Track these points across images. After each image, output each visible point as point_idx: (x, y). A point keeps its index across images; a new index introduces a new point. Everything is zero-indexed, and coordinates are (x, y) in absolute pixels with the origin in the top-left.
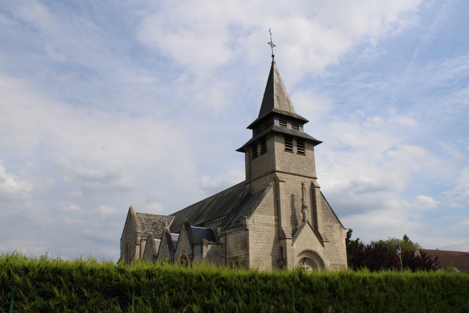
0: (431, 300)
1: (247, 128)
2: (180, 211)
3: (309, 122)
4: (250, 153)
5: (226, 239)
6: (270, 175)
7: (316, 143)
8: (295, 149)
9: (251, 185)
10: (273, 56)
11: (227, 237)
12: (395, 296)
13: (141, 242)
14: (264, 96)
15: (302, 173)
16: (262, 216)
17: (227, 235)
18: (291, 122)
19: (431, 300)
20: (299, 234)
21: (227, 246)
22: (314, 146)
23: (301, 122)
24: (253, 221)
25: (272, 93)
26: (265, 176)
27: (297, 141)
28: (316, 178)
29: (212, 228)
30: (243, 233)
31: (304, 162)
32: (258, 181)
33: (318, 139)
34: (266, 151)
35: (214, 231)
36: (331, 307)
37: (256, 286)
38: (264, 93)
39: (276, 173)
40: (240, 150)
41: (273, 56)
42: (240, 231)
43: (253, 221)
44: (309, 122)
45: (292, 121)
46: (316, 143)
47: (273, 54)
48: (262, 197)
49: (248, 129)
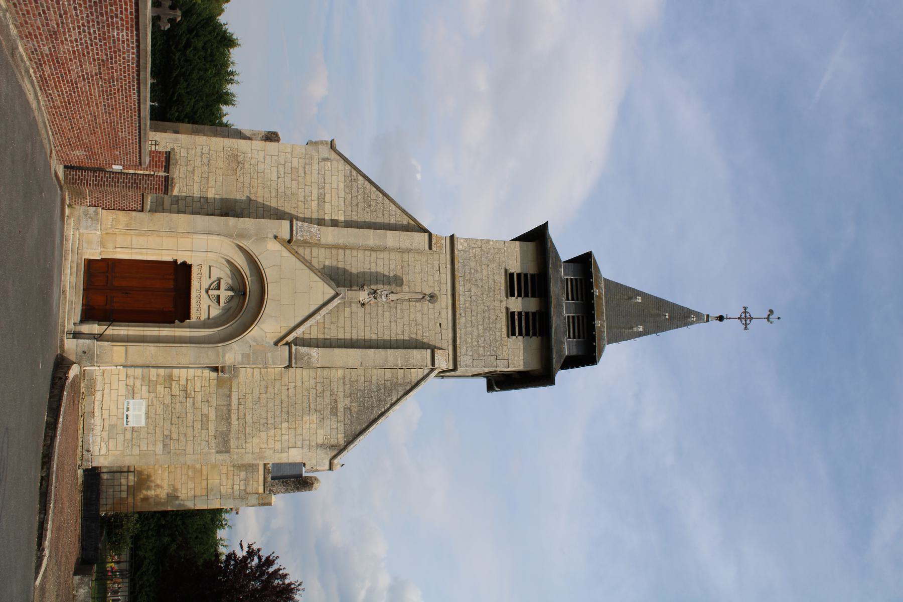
10: (721, 318)
15: (463, 320)
16: (342, 185)
24: (327, 159)
41: (721, 318)
43: (327, 159)
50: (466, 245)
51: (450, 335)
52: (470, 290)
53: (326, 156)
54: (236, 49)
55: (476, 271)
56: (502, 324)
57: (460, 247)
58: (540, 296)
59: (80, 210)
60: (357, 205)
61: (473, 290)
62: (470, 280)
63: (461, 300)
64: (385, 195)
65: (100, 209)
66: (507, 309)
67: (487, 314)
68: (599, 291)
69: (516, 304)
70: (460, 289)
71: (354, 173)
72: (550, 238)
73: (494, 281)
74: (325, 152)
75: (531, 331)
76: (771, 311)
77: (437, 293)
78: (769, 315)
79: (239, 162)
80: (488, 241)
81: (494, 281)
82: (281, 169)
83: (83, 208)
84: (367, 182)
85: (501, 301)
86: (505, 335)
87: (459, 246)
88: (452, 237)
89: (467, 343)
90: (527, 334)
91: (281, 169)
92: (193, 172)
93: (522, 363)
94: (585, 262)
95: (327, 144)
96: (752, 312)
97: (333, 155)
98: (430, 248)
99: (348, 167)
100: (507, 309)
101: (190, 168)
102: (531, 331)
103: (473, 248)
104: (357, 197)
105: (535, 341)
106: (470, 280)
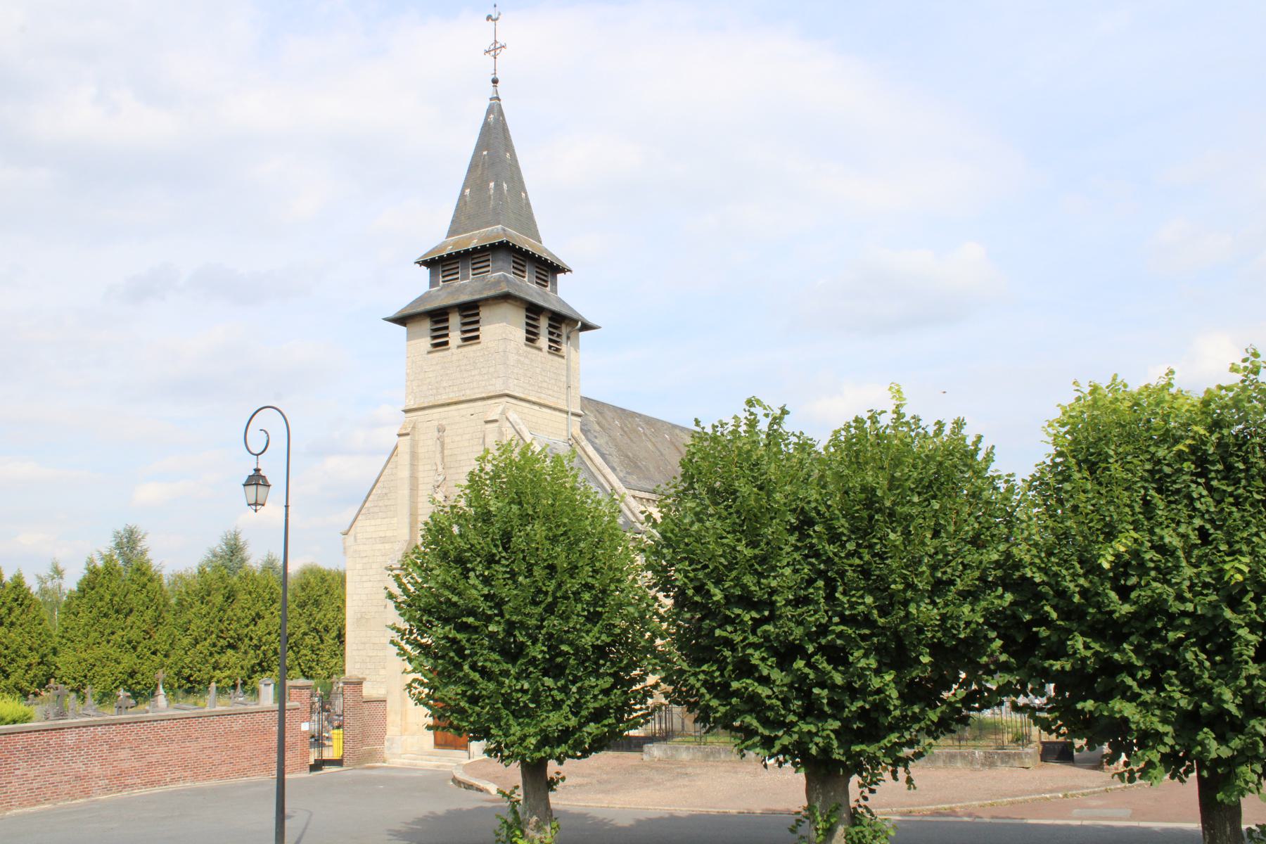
8: (543, 341)
10: (495, 81)
12: (1255, 460)
15: (468, 392)
16: (373, 522)
18: (512, 259)
23: (548, 269)
24: (355, 537)
25: (523, 194)
27: (550, 319)
31: (474, 362)
33: (590, 319)
34: (477, 337)
36: (1009, 597)
37: (658, 668)
41: (495, 81)
43: (355, 537)
45: (514, 257)
46: (586, 327)
49: (424, 268)
50: (410, 397)
51: (480, 403)
52: (444, 388)
53: (353, 538)
54: (25, 580)
55: (429, 384)
56: (471, 349)
57: (412, 402)
58: (447, 314)
59: (387, 754)
60: (386, 506)
61: (445, 385)
62: (437, 389)
63: (454, 397)
64: (377, 481)
65: (386, 737)
66: (459, 347)
67: (463, 368)
68: (474, 239)
69: (455, 337)
70: (443, 398)
71: (363, 511)
72: (399, 312)
73: (437, 364)
74: (350, 539)
75: (475, 319)
76: (489, 18)
77: (436, 423)
78: (492, 20)
79: (362, 617)
80: (407, 374)
81: (437, 364)
82: (364, 578)
83: (386, 751)
84: (370, 499)
85: (453, 354)
86: (478, 347)
87: (412, 405)
88: (406, 411)
89: (486, 386)
90: (447, 328)
91: (364, 578)
92: (370, 657)
93: (501, 324)
94: (439, 264)
95: (345, 538)
96: (488, 44)
97: (352, 532)
98: (408, 434)
99: (360, 517)
100: (459, 347)
101: (368, 660)
102: (475, 319)
103: (413, 389)
104: (380, 507)
105: (484, 313)
106: (437, 389)
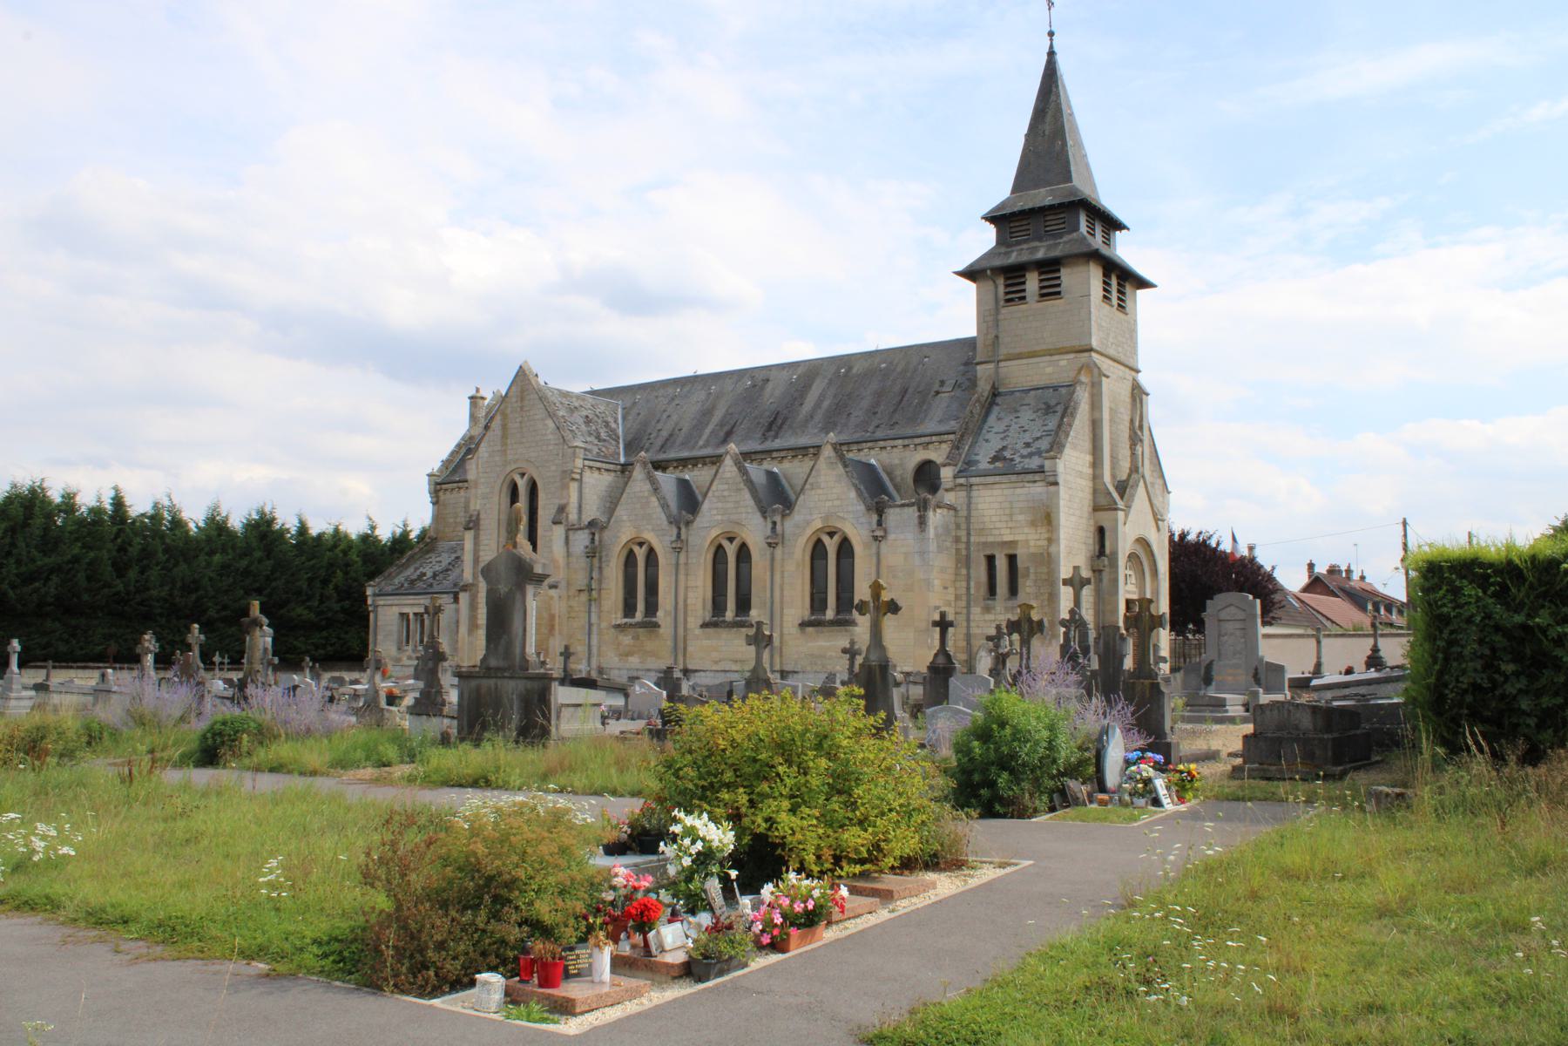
0: (107, 571)
1: (983, 218)
2: (634, 386)
3: (1128, 229)
4: (996, 287)
5: (969, 498)
6: (1072, 356)
7: (1143, 284)
9: (997, 368)
10: (1051, 34)
11: (974, 493)
13: (581, 474)
14: (1026, 140)
17: (975, 488)
19: (107, 571)
20: (1133, 500)
21: (974, 513)
22: (1138, 288)
26: (1051, 355)
28: (1138, 371)
29: (873, 461)
30: (1038, 489)
32: (1024, 361)
35: (880, 470)
38: (1026, 132)
39: (1093, 354)
40: (971, 274)
41: (1051, 34)
42: (1027, 485)
44: (1128, 229)
46: (1143, 284)
47: (1053, 29)
48: (1074, 408)
